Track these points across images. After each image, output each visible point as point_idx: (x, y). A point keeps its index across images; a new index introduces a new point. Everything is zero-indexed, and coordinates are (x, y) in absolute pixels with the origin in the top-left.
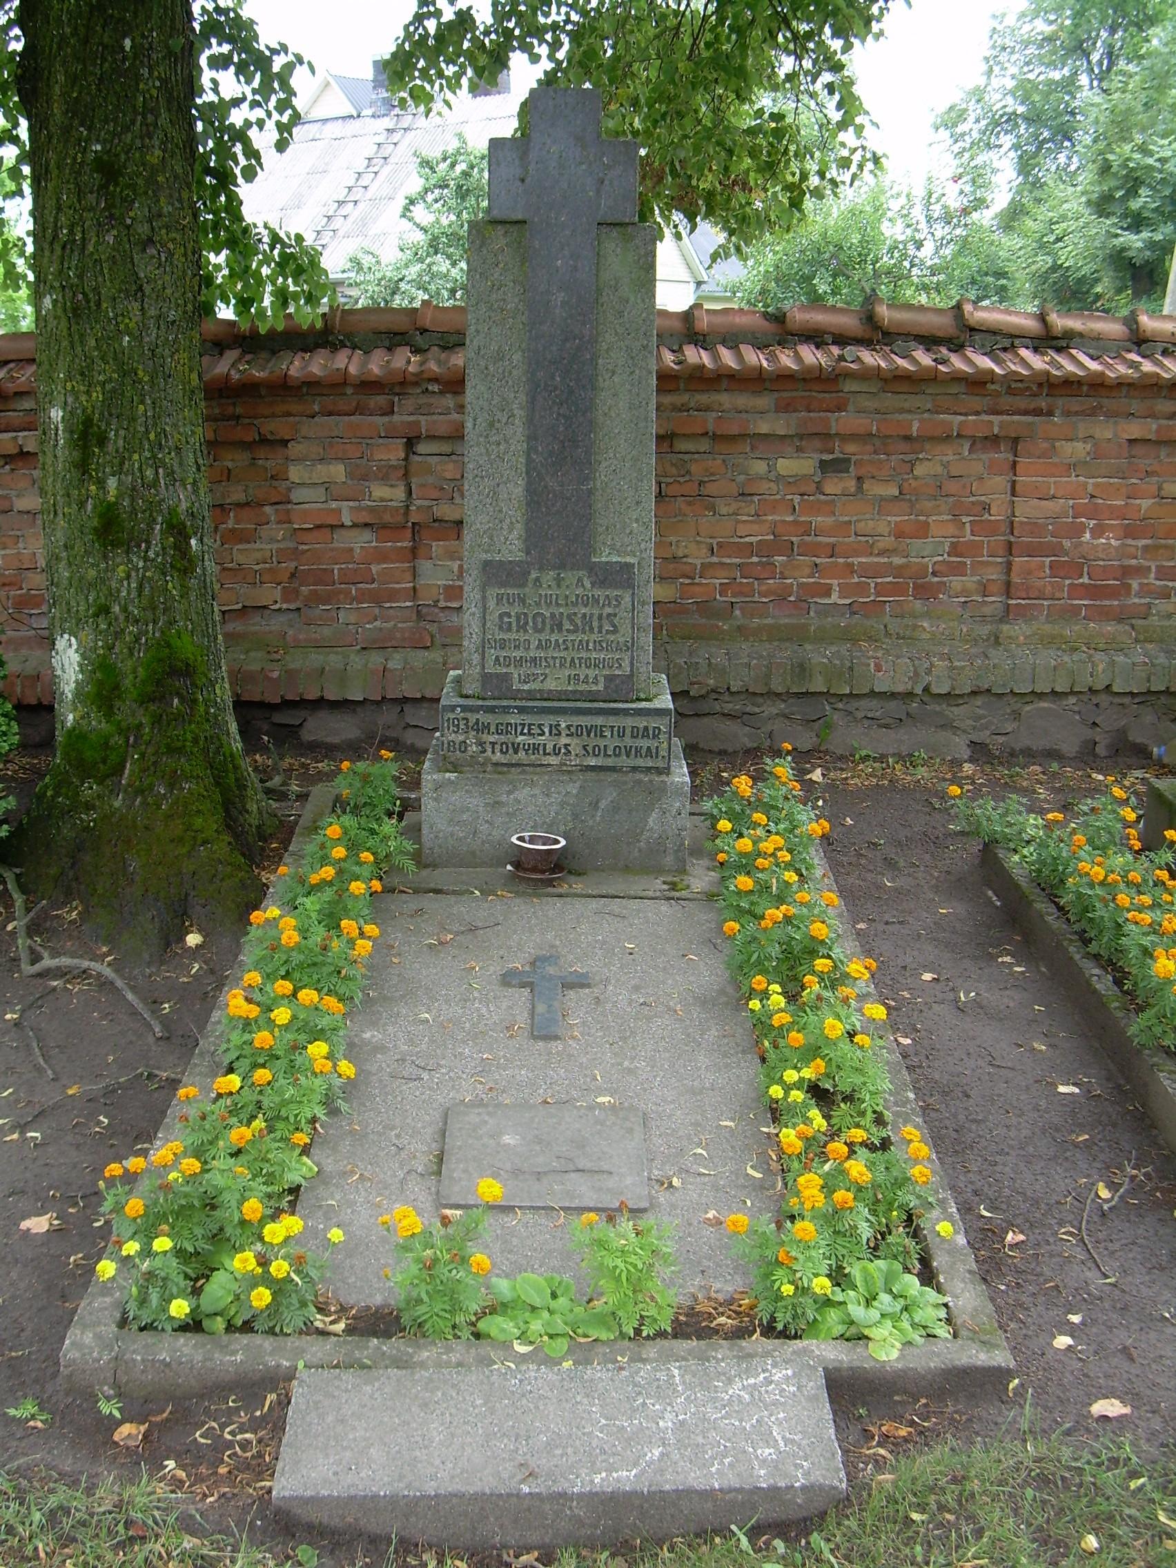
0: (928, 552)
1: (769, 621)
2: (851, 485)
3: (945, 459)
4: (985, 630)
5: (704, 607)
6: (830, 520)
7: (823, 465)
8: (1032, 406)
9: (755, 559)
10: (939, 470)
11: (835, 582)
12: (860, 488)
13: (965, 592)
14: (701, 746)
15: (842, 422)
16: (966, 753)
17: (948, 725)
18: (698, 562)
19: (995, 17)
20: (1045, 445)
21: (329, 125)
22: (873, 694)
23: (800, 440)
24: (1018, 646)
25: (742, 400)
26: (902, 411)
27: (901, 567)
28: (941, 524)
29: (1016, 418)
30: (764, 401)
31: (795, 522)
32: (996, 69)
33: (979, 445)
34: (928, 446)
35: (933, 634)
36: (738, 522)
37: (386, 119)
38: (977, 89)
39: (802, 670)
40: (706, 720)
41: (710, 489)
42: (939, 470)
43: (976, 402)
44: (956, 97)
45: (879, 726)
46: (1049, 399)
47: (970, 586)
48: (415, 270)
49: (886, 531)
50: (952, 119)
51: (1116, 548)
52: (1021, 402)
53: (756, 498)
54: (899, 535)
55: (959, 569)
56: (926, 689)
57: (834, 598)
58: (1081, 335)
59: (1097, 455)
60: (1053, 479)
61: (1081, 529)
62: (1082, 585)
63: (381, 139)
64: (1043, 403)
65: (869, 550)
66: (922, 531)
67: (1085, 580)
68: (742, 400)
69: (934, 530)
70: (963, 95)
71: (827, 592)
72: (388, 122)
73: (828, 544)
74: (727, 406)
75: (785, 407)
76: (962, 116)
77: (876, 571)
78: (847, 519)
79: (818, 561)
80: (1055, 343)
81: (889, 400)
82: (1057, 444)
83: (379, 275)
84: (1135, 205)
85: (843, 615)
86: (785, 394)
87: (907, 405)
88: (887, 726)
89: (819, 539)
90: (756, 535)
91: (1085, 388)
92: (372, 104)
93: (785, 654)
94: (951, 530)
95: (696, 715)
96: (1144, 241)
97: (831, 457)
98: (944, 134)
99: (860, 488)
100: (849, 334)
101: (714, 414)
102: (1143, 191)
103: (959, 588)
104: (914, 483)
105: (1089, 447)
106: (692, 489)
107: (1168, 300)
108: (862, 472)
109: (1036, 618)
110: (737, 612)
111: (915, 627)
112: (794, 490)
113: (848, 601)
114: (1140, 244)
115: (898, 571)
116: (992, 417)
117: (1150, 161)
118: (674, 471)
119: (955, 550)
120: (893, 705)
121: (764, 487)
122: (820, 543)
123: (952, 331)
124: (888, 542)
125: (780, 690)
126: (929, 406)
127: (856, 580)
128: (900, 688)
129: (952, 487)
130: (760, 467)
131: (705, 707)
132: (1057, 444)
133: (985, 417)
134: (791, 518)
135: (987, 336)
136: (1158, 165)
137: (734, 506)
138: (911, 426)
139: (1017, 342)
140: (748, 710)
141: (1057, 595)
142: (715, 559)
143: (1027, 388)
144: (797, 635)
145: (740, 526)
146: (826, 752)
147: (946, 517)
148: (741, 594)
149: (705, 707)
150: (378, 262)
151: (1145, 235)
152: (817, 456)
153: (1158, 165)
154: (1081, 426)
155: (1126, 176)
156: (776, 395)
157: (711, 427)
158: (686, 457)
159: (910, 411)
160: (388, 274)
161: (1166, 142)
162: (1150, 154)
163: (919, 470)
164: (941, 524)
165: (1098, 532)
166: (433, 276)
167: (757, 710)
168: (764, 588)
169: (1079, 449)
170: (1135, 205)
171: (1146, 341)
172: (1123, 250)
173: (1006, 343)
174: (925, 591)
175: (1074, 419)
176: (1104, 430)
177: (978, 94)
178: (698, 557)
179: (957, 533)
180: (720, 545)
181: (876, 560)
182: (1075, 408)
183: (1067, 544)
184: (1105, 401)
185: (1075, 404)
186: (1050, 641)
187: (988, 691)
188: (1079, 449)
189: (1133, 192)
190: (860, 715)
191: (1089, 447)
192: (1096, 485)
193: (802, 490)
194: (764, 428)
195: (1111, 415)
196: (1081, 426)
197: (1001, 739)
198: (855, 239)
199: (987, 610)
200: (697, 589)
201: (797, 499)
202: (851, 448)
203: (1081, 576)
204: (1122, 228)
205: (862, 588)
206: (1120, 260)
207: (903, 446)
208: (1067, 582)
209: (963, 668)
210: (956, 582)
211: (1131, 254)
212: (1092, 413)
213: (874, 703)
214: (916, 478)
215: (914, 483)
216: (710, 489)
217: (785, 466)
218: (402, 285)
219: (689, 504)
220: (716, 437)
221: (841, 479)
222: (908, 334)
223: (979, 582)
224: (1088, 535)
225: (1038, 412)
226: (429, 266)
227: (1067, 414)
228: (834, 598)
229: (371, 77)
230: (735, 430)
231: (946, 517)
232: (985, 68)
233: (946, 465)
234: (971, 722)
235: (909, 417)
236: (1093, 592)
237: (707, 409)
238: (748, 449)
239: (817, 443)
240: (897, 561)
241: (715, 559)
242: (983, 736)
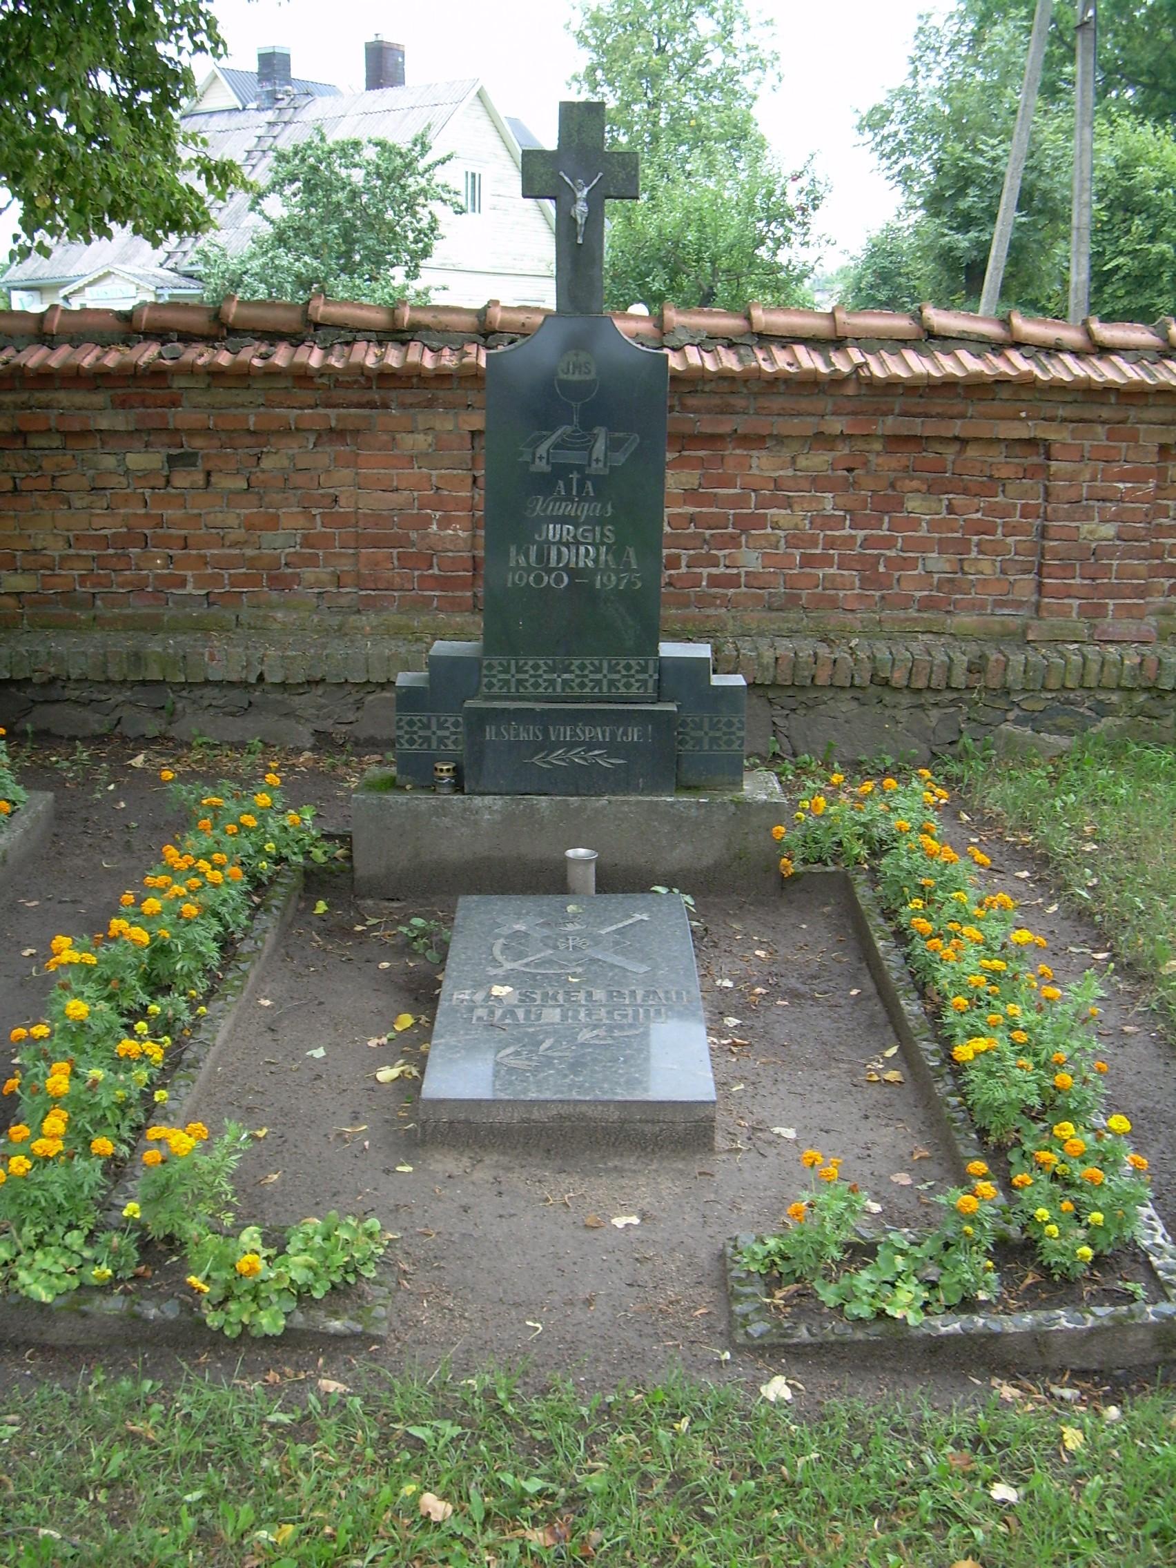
0: (279, 545)
1: (129, 611)
2: (200, 479)
3: (290, 452)
4: (335, 621)
5: (67, 597)
6: (180, 513)
7: (172, 460)
8: (364, 400)
9: (111, 551)
10: (286, 463)
11: (189, 573)
12: (208, 482)
13: (318, 584)
14: (53, 730)
15: (180, 417)
16: (309, 741)
17: (290, 714)
18: (56, 554)
19: (921, 17)
20: (385, 437)
21: (215, 118)
22: (207, 683)
23: (144, 434)
24: (364, 636)
25: (79, 398)
26: (238, 406)
27: (252, 558)
28: (290, 516)
29: (353, 411)
30: (99, 399)
31: (147, 515)
32: (923, 71)
33: (325, 439)
34: (272, 440)
35: (284, 624)
36: (92, 515)
37: (270, 112)
38: (903, 90)
39: (137, 658)
40: (57, 707)
41: (63, 483)
42: (286, 463)
43: (308, 396)
44: (881, 98)
45: (225, 714)
46: (382, 392)
47: (325, 577)
48: (255, 265)
49: (235, 523)
50: (875, 120)
51: (464, 540)
52: (354, 395)
53: (108, 492)
54: (250, 527)
55: (312, 561)
56: (261, 678)
57: (189, 589)
58: (428, 328)
59: (439, 446)
60: (394, 472)
61: (428, 521)
62: (431, 576)
63: (260, 132)
64: (376, 396)
65: (222, 542)
66: (273, 523)
67: (436, 571)
68: (80, 398)
69: (284, 522)
70: (887, 96)
71: (183, 583)
72: (270, 116)
73: (179, 537)
74: (65, 403)
75: (122, 404)
76: (886, 116)
77: (228, 563)
78: (196, 511)
79: (171, 552)
80: (399, 336)
81: (221, 395)
82: (398, 436)
83: (223, 267)
84: (963, 204)
85: (201, 605)
86: (120, 391)
87: (239, 400)
88: (232, 714)
89: (172, 531)
90: (110, 527)
91: (415, 380)
92: (257, 97)
93: (125, 643)
94: (302, 522)
95: (46, 702)
96: (970, 240)
97: (179, 451)
98: (869, 135)
99: (208, 482)
100: (195, 331)
101: (56, 412)
102: (972, 191)
103: (312, 580)
104: (261, 476)
105: (430, 439)
106: (45, 483)
107: (983, 300)
108: (210, 466)
109: (386, 609)
110: (99, 603)
111: (266, 618)
112: (144, 483)
113: (203, 592)
114: (966, 244)
115: (251, 562)
116: (328, 411)
117: (981, 161)
118: (26, 466)
119: (307, 542)
120: (235, 694)
121: (114, 481)
122: (170, 536)
123: (296, 327)
124: (239, 534)
125: (117, 678)
126: (261, 401)
127: (210, 571)
128: (234, 677)
129: (298, 479)
130: (109, 462)
131: (54, 693)
132: (398, 436)
133: (322, 411)
134: (143, 511)
135: (331, 330)
136: (988, 164)
137: (87, 500)
138: (247, 420)
139: (359, 336)
140: (94, 696)
141: (407, 586)
142: (72, 552)
143: (356, 382)
144: (152, 625)
145: (95, 519)
146: (172, 739)
147: (295, 510)
148: (100, 584)
149: (54, 693)
150: (224, 255)
151: (973, 234)
152: (165, 451)
153: (988, 164)
154: (420, 418)
155: (957, 175)
156: (111, 392)
157: (53, 423)
158: (38, 453)
159: (243, 406)
160: (232, 267)
161: (996, 142)
162: (981, 153)
163: (266, 463)
164: (290, 516)
165: (445, 523)
166: (277, 268)
167: (103, 697)
168: (120, 579)
169: (421, 441)
170: (963, 204)
171: (494, 332)
172: (951, 249)
173: (349, 337)
174: (279, 582)
175: (412, 411)
176: (444, 423)
177: (906, 95)
178: (56, 549)
179: (307, 525)
180: (77, 538)
181: (227, 551)
182: (409, 400)
183: (414, 535)
184: (441, 394)
185: (409, 397)
186: (396, 632)
187: (323, 680)
188: (421, 441)
189: (961, 192)
190: (206, 703)
191: (430, 439)
192: (441, 477)
193: (152, 484)
194: (104, 424)
195: (449, 406)
196: (420, 418)
197: (344, 728)
198: (691, 236)
199: (344, 601)
200: (57, 580)
201: (148, 492)
202: (198, 442)
203: (431, 567)
204: (951, 228)
205: (216, 579)
206: (947, 258)
207: (249, 440)
208: (416, 573)
209: (294, 657)
210: (309, 574)
211: (958, 253)
212: (430, 404)
213: (216, 692)
214: (263, 471)
215: (261, 476)
216: (63, 483)
217: (135, 460)
218: (246, 279)
219: (45, 498)
220: (66, 434)
221: (189, 473)
222: (254, 331)
223: (333, 573)
224: (435, 527)
225: (371, 405)
226: (272, 259)
227: (403, 406)
228: (189, 589)
229: (256, 70)
230: (77, 427)
231: (295, 510)
232: (911, 68)
233: (292, 458)
234: (314, 711)
235: (245, 411)
236: (443, 583)
237: (47, 406)
238: (98, 444)
239: (165, 438)
240: (249, 552)
241: (72, 552)
242: (327, 726)
